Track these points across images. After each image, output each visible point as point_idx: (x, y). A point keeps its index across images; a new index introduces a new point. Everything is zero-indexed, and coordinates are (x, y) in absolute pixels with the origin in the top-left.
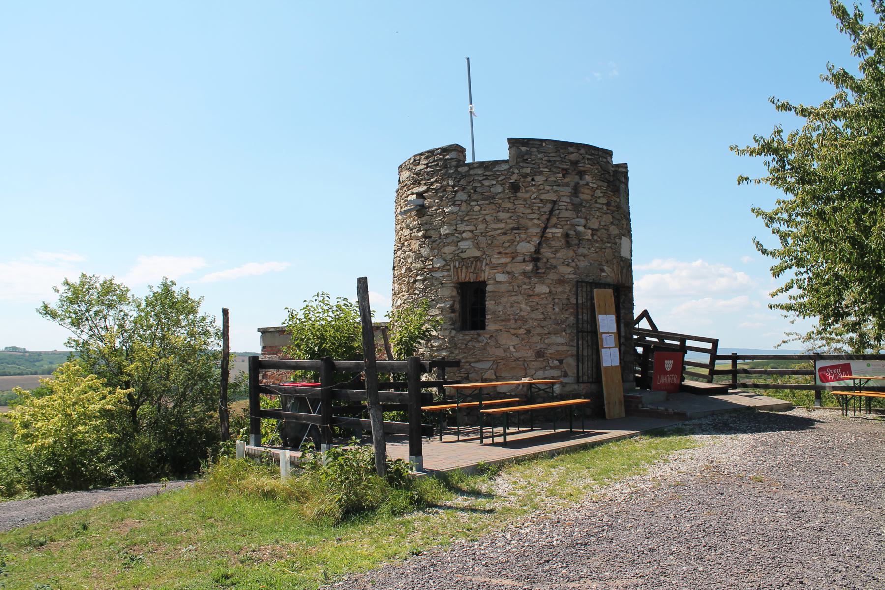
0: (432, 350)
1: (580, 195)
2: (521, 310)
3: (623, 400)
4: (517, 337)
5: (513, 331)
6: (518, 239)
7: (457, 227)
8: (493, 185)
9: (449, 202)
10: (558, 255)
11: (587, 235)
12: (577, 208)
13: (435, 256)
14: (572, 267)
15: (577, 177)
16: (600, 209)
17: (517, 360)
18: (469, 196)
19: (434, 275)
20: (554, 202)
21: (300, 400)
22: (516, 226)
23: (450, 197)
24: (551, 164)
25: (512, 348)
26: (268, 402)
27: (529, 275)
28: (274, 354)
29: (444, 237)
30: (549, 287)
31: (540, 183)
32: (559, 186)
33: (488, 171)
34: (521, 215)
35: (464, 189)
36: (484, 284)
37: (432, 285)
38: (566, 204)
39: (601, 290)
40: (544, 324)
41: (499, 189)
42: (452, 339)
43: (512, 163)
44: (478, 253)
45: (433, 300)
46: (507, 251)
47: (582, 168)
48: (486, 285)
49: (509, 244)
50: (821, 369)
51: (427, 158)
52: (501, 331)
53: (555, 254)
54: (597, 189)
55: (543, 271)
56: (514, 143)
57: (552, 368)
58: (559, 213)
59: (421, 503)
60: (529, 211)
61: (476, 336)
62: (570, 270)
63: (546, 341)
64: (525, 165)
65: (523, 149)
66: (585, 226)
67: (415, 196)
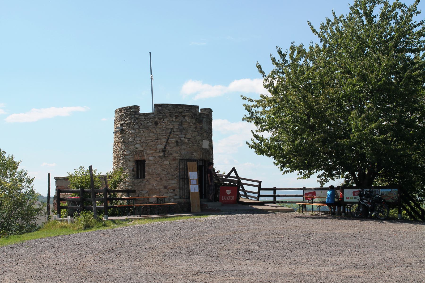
0: (126, 186)
2: (158, 171)
3: (200, 205)
5: (155, 179)
6: (157, 143)
9: (132, 129)
10: (173, 149)
11: (186, 141)
12: (181, 131)
13: (127, 150)
14: (179, 154)
15: (182, 118)
16: (192, 130)
17: (157, 190)
18: (139, 127)
19: (127, 157)
20: (172, 129)
21: (73, 202)
22: (156, 138)
23: (132, 127)
24: (171, 114)
25: (155, 185)
26: (63, 204)
29: (130, 142)
30: (169, 162)
32: (174, 122)
33: (146, 117)
34: (159, 134)
35: (137, 124)
36: (144, 161)
38: (177, 129)
39: (191, 163)
41: (150, 124)
42: (133, 182)
44: (142, 149)
45: (126, 167)
47: (184, 115)
48: (145, 161)
49: (153, 146)
51: (124, 110)
52: (150, 178)
53: (172, 149)
54: (191, 122)
55: (167, 156)
57: (170, 192)
58: (174, 133)
59: (105, 225)
62: (178, 155)
64: (160, 114)
65: (160, 108)
66: (185, 137)
67: (120, 125)
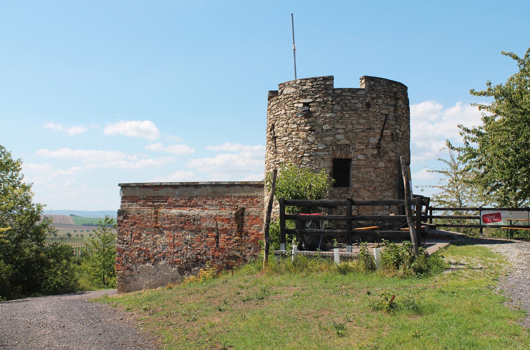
1: (397, 112)
4: (369, 191)
5: (367, 188)
6: (370, 135)
7: (334, 126)
8: (356, 103)
9: (329, 110)
10: (389, 145)
13: (319, 142)
14: (395, 153)
20: (387, 115)
22: (369, 127)
27: (376, 156)
28: (134, 202)
29: (325, 131)
31: (380, 103)
32: (389, 106)
34: (372, 122)
36: (350, 160)
37: (316, 159)
38: (392, 116)
40: (382, 184)
41: (360, 105)
43: (367, 91)
44: (348, 142)
46: (364, 142)
47: (398, 96)
49: (365, 138)
50: (484, 216)
51: (312, 82)
56: (368, 79)
58: (389, 122)
60: (375, 119)
61: (346, 191)
63: (383, 194)
64: (373, 92)
65: (372, 83)
